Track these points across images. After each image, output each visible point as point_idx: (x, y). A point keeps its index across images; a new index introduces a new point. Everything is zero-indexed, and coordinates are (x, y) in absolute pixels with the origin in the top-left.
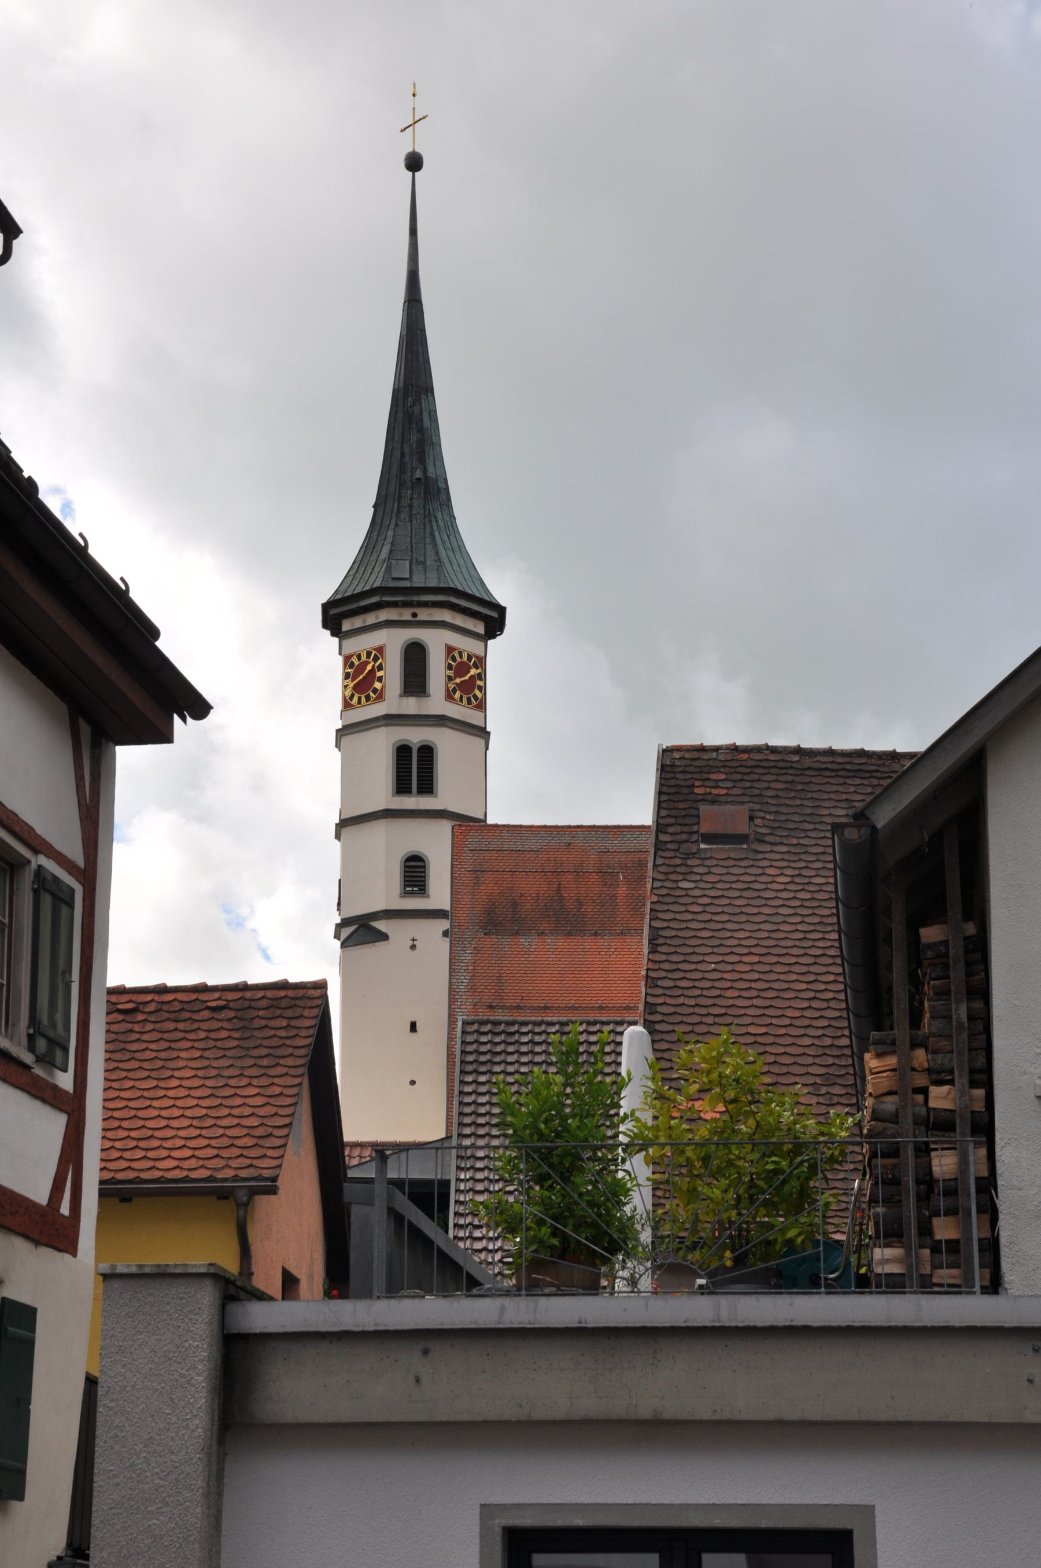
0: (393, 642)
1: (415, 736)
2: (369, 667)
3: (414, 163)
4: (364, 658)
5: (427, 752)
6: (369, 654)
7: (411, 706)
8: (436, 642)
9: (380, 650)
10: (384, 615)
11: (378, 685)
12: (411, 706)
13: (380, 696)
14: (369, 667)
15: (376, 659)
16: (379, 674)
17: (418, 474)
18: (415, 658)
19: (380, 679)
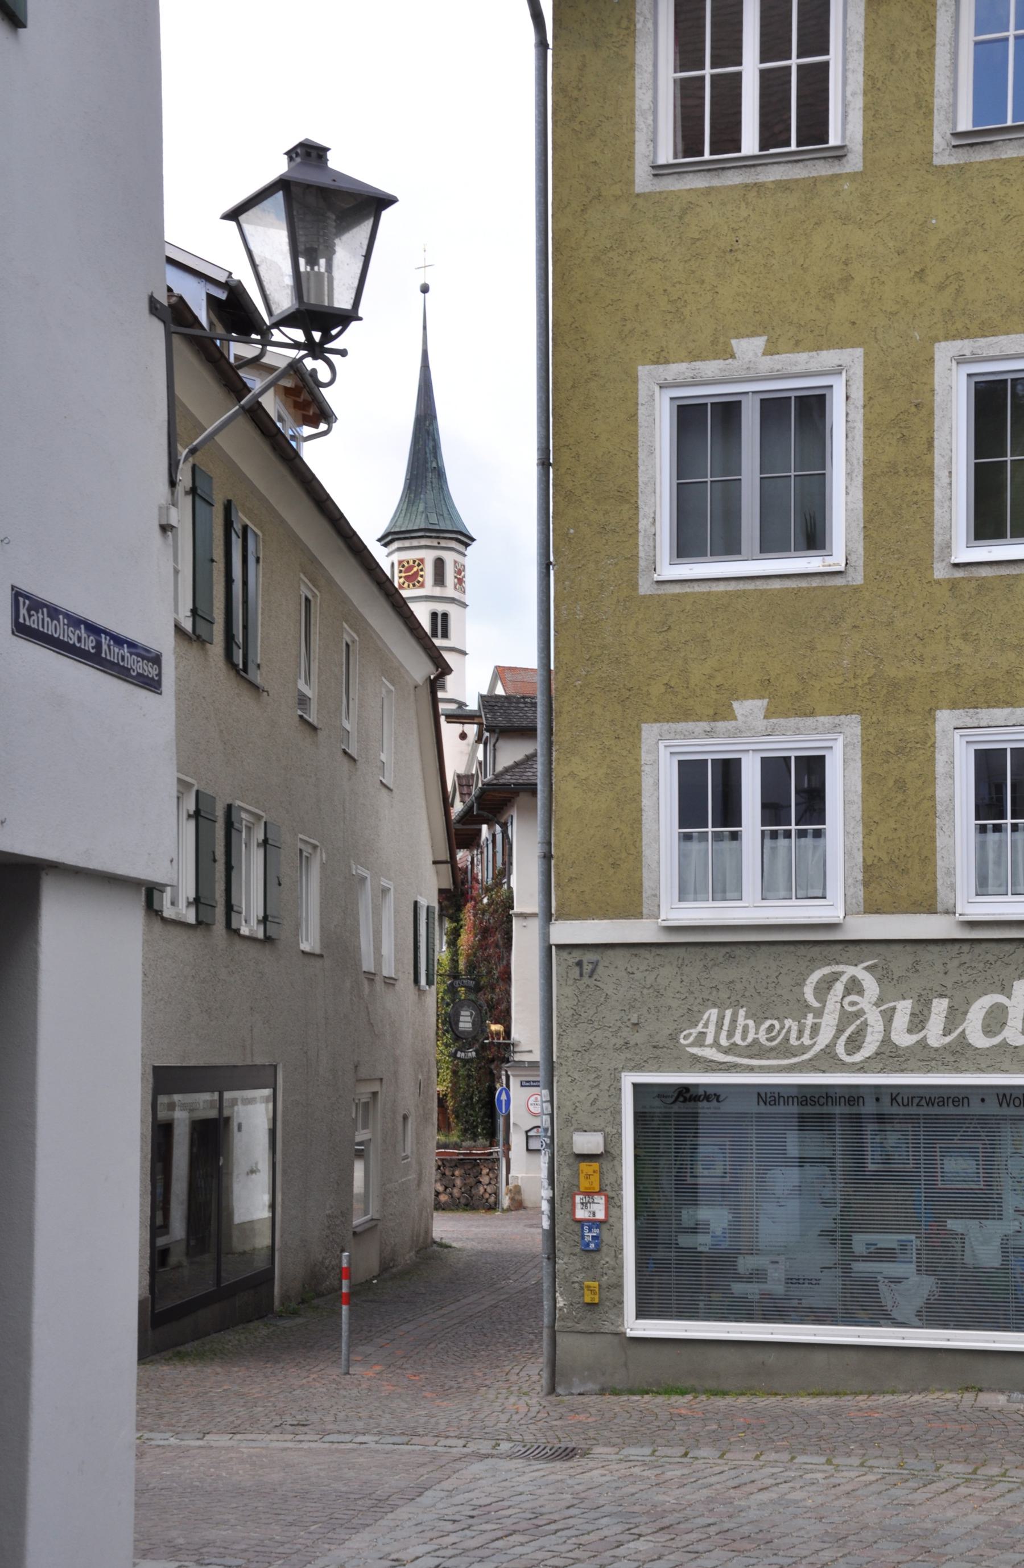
0: (429, 557)
1: (440, 608)
2: (415, 569)
3: (425, 289)
4: (411, 563)
5: (445, 616)
6: (414, 562)
7: (437, 591)
8: (449, 557)
9: (422, 561)
10: (423, 542)
11: (420, 579)
12: (437, 591)
13: (422, 585)
14: (415, 569)
15: (419, 565)
16: (421, 573)
17: (434, 465)
18: (439, 563)
19: (422, 576)
